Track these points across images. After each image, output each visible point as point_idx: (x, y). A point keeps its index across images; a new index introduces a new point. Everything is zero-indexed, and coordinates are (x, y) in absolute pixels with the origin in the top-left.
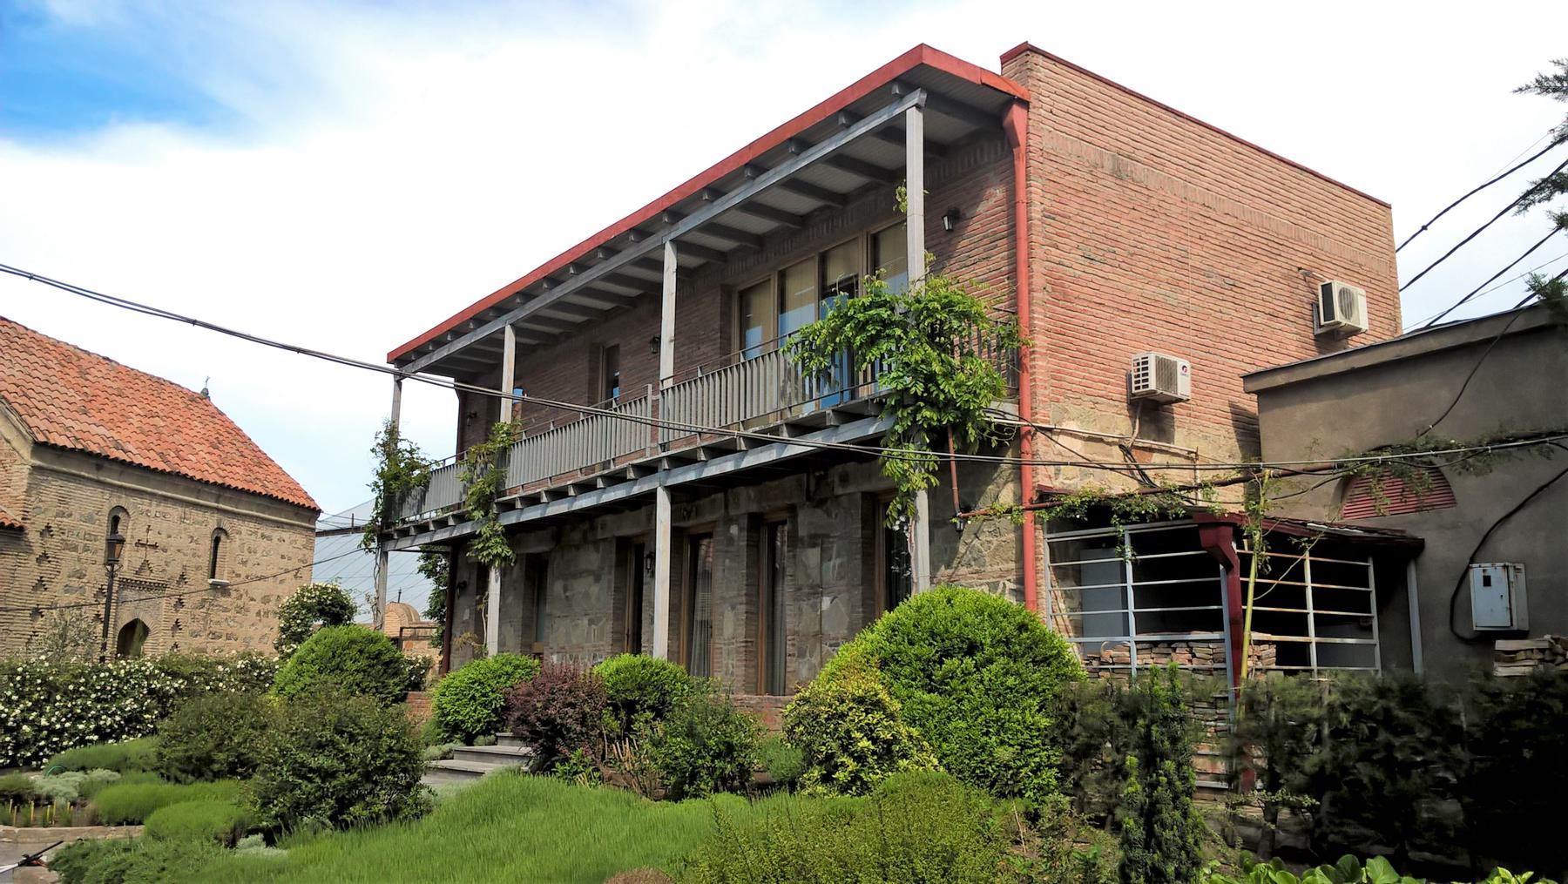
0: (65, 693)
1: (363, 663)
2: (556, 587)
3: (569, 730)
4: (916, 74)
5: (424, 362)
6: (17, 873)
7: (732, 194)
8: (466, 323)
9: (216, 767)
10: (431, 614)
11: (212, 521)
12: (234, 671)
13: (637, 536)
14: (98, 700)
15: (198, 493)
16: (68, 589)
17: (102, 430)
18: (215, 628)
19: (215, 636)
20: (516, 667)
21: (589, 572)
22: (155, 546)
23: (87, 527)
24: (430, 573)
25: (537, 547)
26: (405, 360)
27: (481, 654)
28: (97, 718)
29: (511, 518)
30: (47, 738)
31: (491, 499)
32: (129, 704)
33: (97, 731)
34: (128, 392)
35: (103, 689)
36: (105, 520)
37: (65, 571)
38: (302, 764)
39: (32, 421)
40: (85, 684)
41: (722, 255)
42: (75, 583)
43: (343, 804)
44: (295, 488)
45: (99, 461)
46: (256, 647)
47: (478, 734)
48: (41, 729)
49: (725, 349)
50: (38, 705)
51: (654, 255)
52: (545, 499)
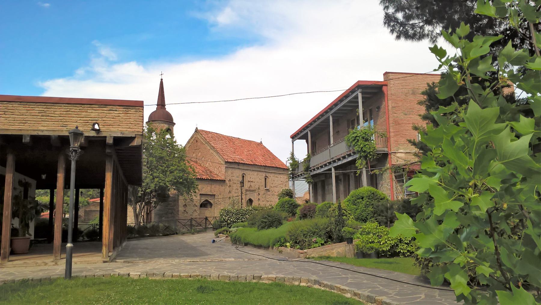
1: (288, 206)
4: (361, 86)
8: (332, 106)
11: (264, 174)
19: (268, 201)
26: (294, 137)
39: (224, 157)
42: (236, 191)
45: (238, 164)
50: (230, 217)
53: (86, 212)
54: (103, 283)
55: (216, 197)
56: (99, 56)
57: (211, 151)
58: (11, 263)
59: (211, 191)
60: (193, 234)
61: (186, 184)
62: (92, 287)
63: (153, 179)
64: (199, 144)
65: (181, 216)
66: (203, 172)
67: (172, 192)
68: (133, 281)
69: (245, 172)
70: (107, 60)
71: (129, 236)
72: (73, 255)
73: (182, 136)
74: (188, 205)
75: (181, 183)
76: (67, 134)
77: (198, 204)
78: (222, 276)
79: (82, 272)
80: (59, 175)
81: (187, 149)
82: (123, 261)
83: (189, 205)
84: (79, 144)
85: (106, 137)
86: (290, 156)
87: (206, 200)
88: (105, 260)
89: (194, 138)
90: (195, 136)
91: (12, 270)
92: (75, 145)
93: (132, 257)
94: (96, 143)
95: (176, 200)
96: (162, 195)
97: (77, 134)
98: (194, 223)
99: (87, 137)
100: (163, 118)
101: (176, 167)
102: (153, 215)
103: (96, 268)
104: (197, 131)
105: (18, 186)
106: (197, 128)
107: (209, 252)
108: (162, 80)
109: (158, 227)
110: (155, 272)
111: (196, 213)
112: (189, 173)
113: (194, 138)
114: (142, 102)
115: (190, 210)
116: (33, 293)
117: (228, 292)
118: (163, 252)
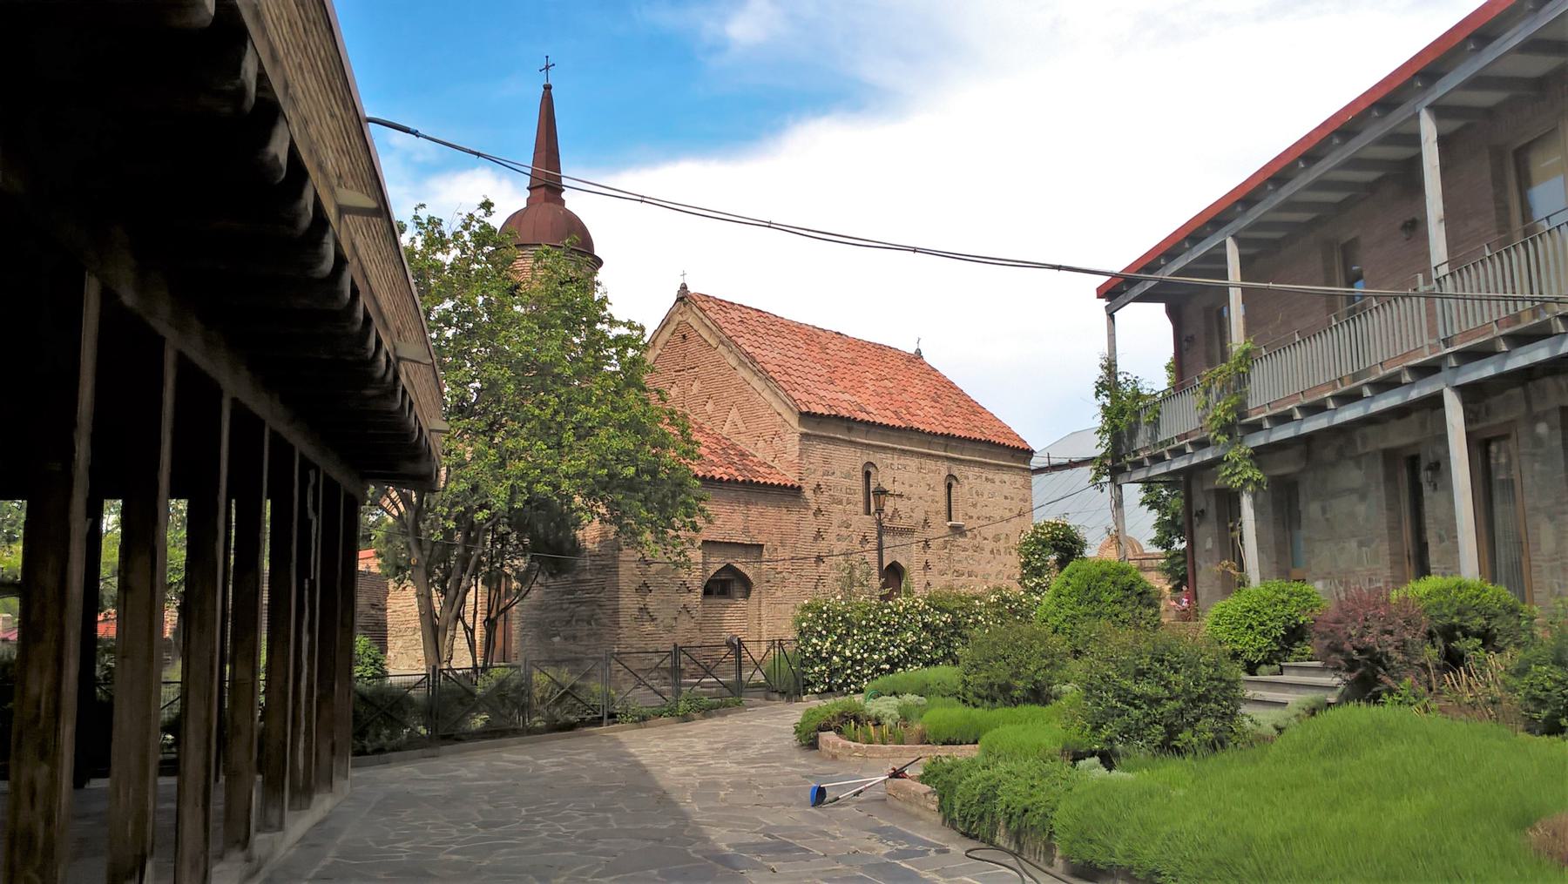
0: (860, 627)
1: (1118, 594)
2: (1311, 509)
3: (1389, 659)
5: (1137, 291)
6: (889, 783)
7: (1508, 34)
9: (1016, 693)
10: (1157, 542)
11: (943, 469)
12: (989, 605)
13: (1407, 447)
14: (885, 634)
15: (930, 445)
16: (839, 538)
17: (846, 396)
18: (958, 567)
19: (959, 574)
20: (1291, 594)
21: (1352, 491)
22: (901, 496)
23: (847, 482)
24: (1153, 505)
25: (1286, 467)
27: (1234, 583)
28: (886, 649)
29: (1259, 440)
30: (851, 667)
31: (1237, 425)
32: (909, 636)
33: (888, 661)
34: (859, 360)
35: (888, 623)
36: (860, 475)
37: (836, 522)
38: (1127, 691)
39: (796, 395)
40: (874, 619)
41: (1489, 112)
42: (844, 532)
43: (1172, 732)
44: (1009, 432)
46: (1005, 583)
47: (1260, 663)
48: (846, 659)
49: (1504, 225)
51: (1405, 129)
52: (1298, 416)
55: (766, 556)
57: (743, 373)
59: (746, 530)
60: (686, 718)
61: (655, 490)
64: (693, 346)
65: (631, 635)
66: (713, 452)
67: (590, 533)
69: (875, 457)
74: (653, 583)
75: (630, 486)
77: (698, 584)
83: (661, 586)
86: (1097, 373)
89: (672, 327)
90: (678, 318)
95: (607, 564)
102: (515, 626)
104: (684, 297)
106: (684, 287)
108: (548, 88)
112: (662, 443)
113: (672, 327)
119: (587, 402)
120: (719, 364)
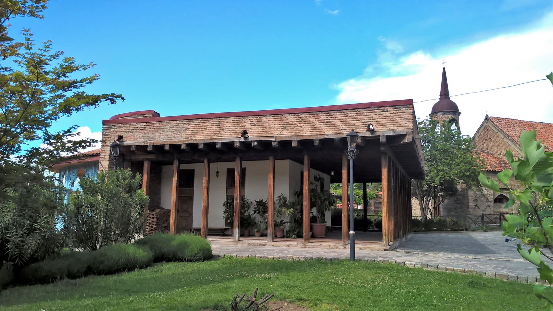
53: (375, 204)
54: (381, 268)
56: (386, 50)
57: (505, 140)
58: (311, 244)
60: (485, 231)
62: (371, 270)
63: (438, 172)
64: (490, 132)
65: (472, 211)
66: (496, 163)
67: (460, 186)
68: (408, 269)
70: (393, 52)
71: (415, 229)
72: (356, 241)
73: (468, 126)
74: (481, 199)
75: (469, 177)
76: (345, 136)
77: (492, 199)
78: (498, 275)
79: (365, 257)
80: (343, 171)
81: (477, 138)
82: (403, 251)
84: (355, 144)
85: (379, 136)
87: (502, 195)
88: (386, 248)
90: (485, 124)
91: (312, 250)
92: (351, 146)
93: (413, 249)
94: (371, 142)
95: (465, 195)
96: (449, 188)
97: (353, 136)
98: (486, 219)
99: (363, 138)
100: (446, 107)
101: (461, 159)
102: (441, 209)
103: (377, 255)
104: (487, 118)
105: (313, 181)
106: (487, 115)
107: (497, 251)
108: (444, 68)
109: (445, 221)
110: (430, 263)
111: (490, 209)
114: (412, 100)
115: (482, 205)
116: (325, 269)
117: (502, 290)
118: (446, 246)
119: (457, 158)
120: (498, 137)
